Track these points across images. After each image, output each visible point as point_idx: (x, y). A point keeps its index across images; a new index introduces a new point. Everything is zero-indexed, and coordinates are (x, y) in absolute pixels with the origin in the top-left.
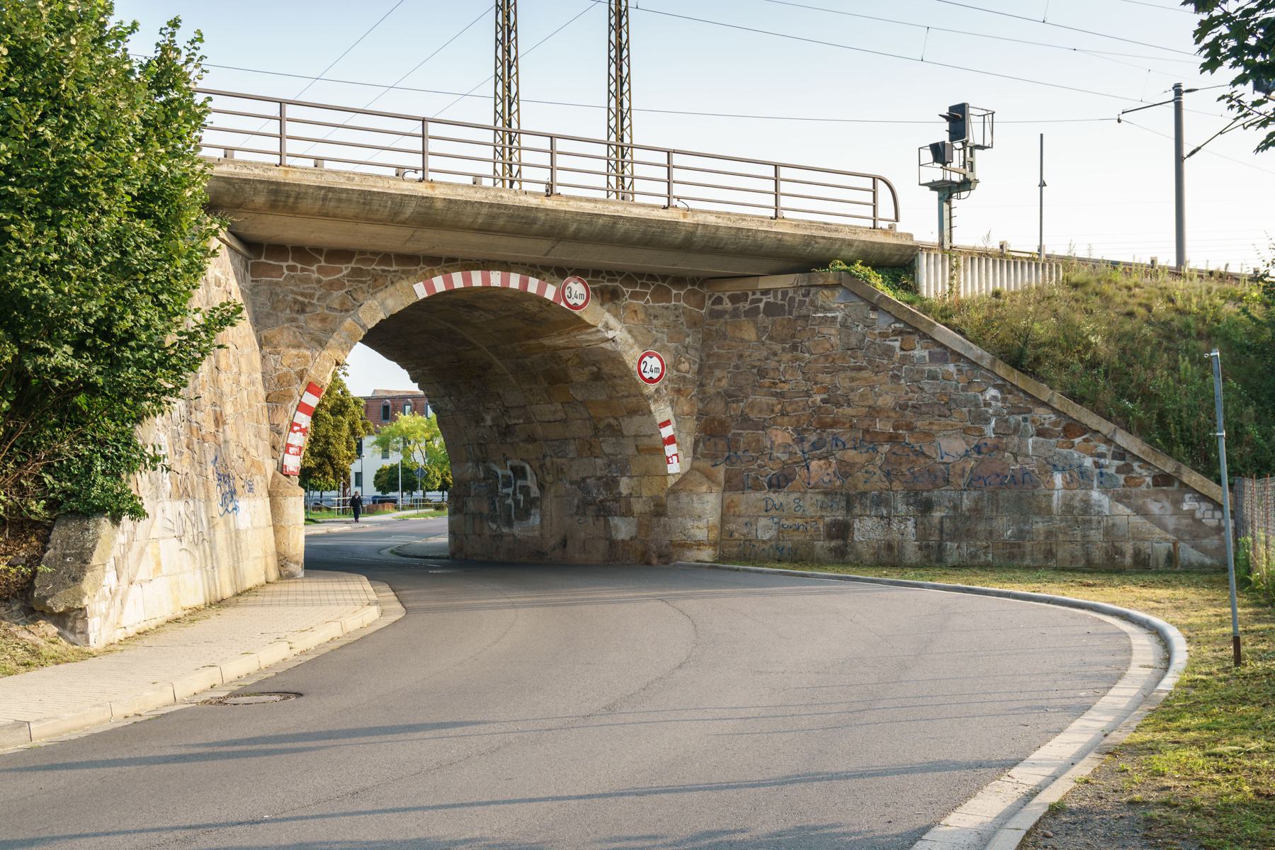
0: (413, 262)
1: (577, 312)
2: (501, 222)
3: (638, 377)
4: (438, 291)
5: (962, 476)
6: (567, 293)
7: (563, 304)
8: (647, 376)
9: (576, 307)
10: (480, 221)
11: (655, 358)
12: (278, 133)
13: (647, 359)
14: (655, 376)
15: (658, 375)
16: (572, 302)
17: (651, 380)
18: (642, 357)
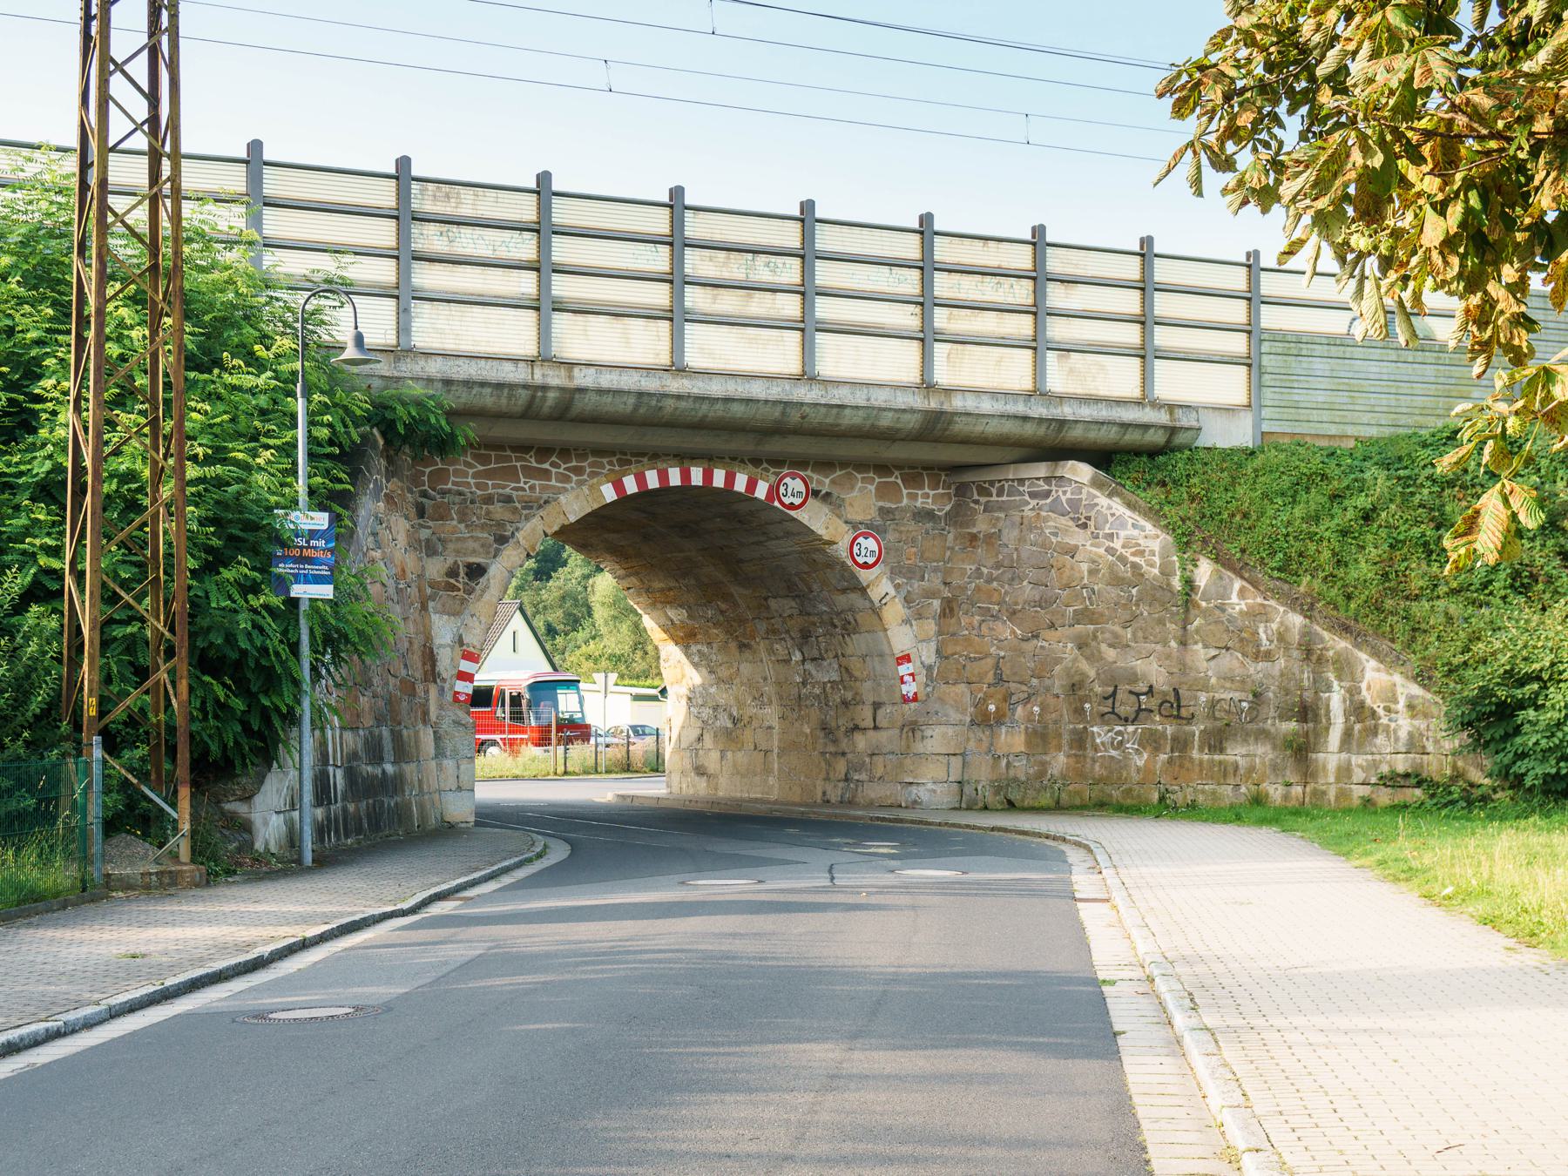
0: (628, 457)
1: (792, 513)
2: (852, 1085)
3: (849, 562)
4: (672, 484)
5: (59, 661)
6: (782, 490)
7: (776, 504)
8: (860, 560)
9: (792, 506)
10: (642, 411)
11: (798, 480)
12: (126, 68)
13: (861, 540)
14: (871, 560)
15: (874, 559)
16: (787, 501)
17: (866, 566)
18: (855, 539)
